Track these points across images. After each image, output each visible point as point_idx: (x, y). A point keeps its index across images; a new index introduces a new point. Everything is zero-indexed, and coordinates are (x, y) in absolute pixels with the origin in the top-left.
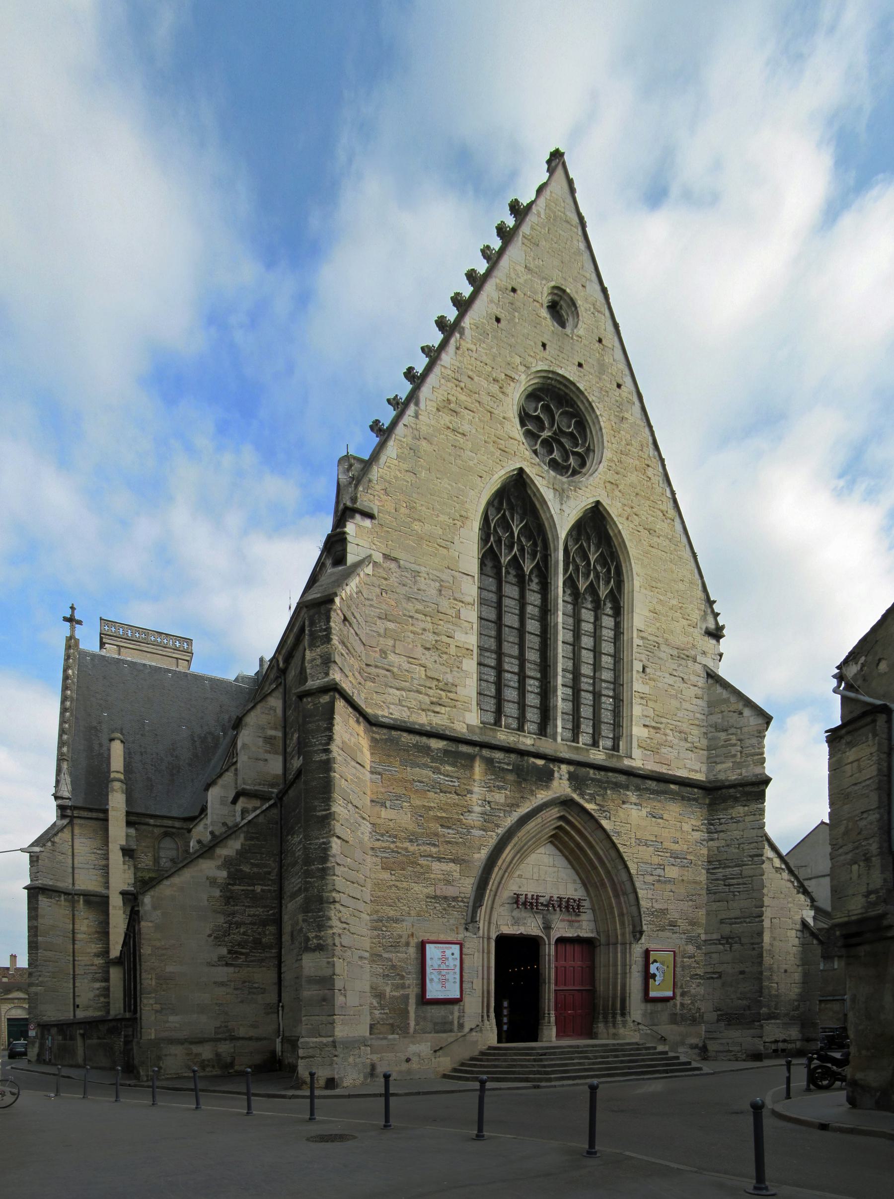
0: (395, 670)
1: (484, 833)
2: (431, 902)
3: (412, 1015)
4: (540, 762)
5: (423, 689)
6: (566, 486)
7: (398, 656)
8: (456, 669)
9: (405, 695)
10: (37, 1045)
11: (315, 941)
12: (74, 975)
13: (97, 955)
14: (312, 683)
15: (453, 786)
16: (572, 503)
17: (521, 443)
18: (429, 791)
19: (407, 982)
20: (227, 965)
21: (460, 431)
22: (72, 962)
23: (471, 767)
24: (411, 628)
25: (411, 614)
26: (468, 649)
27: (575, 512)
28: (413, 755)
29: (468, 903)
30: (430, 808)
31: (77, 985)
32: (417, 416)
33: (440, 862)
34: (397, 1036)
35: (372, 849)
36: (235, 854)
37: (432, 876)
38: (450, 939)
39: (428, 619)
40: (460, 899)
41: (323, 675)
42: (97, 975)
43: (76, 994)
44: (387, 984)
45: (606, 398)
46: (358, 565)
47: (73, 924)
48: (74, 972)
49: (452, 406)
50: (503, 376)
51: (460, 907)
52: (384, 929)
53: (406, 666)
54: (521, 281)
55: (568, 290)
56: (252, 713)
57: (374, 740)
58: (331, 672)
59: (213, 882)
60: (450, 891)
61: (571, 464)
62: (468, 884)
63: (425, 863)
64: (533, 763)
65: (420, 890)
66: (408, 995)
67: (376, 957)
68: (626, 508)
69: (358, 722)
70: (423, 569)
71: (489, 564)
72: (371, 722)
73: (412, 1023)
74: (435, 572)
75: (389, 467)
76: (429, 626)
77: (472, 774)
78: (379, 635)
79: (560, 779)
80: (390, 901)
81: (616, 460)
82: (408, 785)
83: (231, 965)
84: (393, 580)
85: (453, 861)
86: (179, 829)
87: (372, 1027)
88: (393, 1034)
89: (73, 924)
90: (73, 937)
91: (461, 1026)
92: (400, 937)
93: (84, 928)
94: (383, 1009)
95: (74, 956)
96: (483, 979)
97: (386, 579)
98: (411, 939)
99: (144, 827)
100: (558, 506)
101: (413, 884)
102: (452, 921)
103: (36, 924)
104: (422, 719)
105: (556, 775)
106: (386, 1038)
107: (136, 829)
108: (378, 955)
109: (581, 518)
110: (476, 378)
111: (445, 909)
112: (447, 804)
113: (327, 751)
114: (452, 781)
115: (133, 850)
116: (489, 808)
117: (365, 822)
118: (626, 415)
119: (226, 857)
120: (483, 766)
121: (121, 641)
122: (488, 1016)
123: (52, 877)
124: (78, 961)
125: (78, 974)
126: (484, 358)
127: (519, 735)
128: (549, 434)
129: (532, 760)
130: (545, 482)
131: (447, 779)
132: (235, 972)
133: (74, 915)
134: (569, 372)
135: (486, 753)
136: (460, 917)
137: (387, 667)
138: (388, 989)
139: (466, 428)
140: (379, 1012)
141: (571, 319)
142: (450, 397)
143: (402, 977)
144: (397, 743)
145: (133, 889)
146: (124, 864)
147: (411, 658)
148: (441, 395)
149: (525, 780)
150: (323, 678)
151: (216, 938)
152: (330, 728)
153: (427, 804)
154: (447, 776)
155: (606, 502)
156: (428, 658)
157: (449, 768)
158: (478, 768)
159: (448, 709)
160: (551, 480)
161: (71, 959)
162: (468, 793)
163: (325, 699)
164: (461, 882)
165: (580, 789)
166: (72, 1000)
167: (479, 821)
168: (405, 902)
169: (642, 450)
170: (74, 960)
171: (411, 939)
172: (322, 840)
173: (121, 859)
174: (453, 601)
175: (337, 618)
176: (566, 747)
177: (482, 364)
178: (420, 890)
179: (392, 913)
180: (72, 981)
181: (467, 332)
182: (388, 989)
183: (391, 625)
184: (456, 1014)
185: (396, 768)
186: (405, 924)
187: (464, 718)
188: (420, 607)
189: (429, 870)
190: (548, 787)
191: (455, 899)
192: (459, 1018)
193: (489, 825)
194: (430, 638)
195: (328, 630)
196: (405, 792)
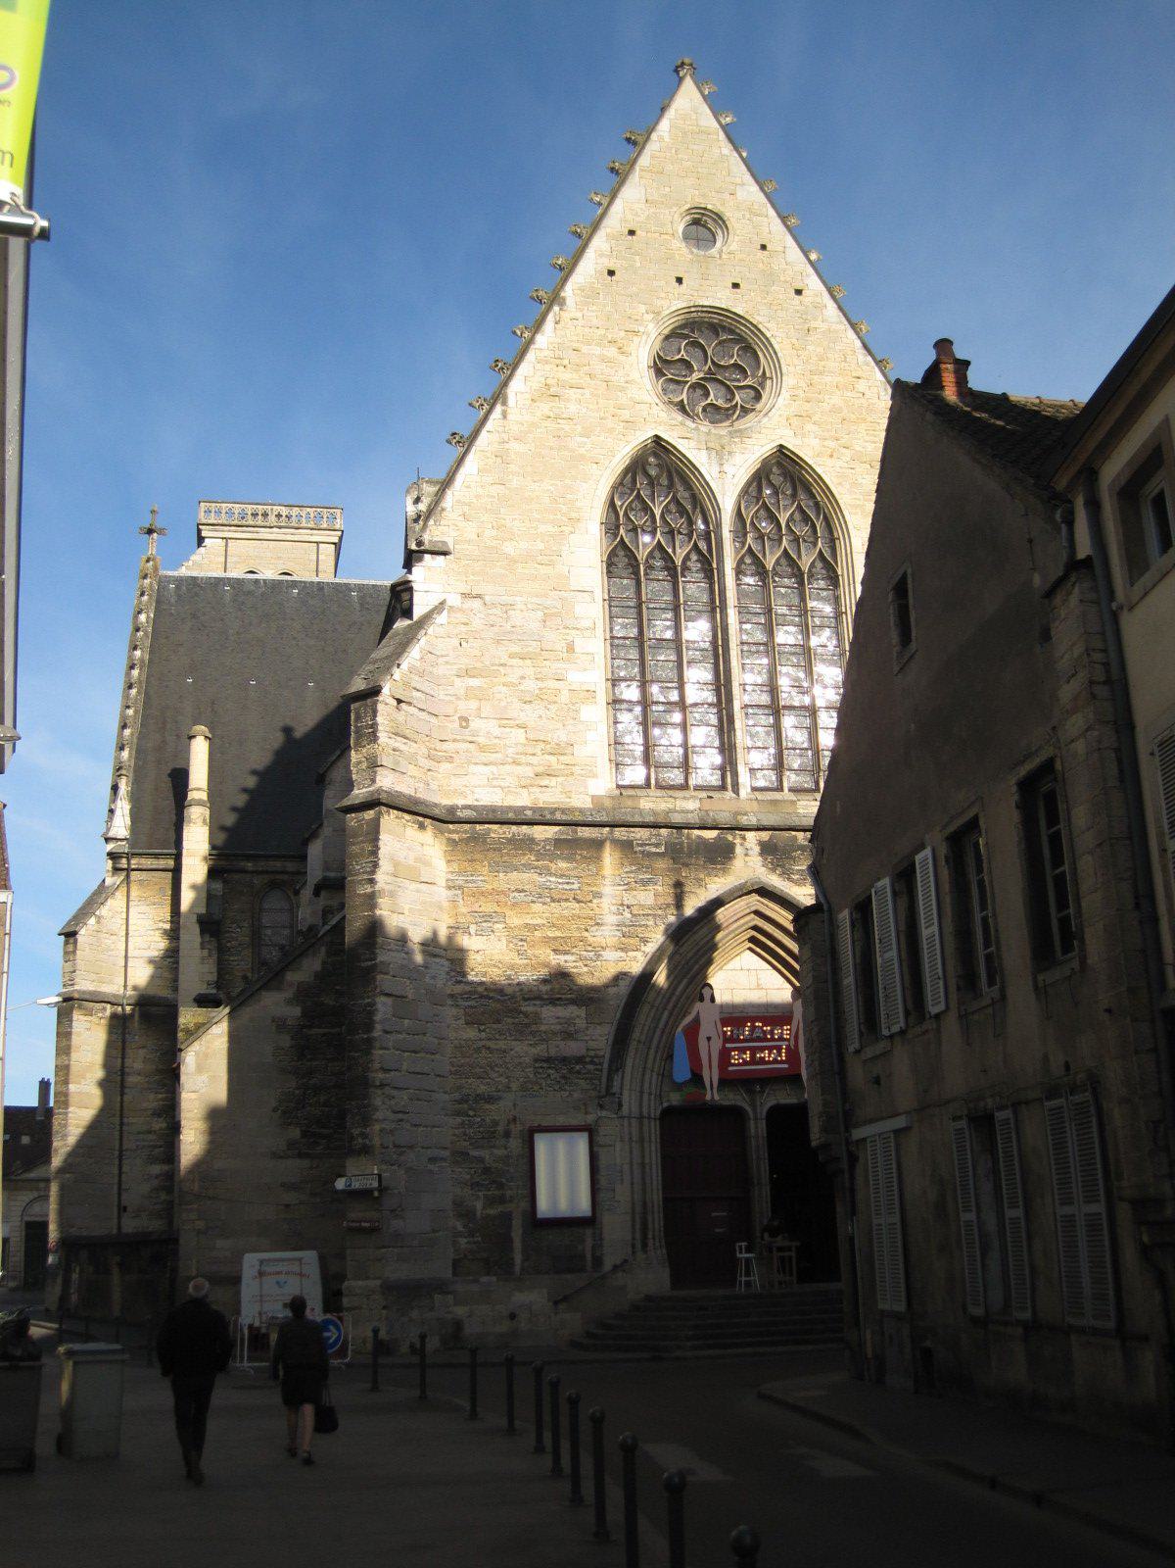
0: (481, 740)
1: (623, 954)
2: (541, 1067)
3: (517, 1244)
4: (710, 835)
5: (523, 759)
6: (725, 441)
7: (486, 721)
8: (571, 722)
9: (495, 772)
10: (59, 1280)
11: (360, 1140)
12: (121, 1151)
13: (157, 1114)
14: (359, 793)
15: (571, 890)
16: (738, 459)
17: (654, 405)
18: (533, 902)
19: (509, 1193)
20: (300, 1156)
21: (564, 416)
22: (118, 1127)
23: (599, 858)
24: (503, 680)
25: (502, 661)
26: (588, 691)
27: (743, 470)
28: (508, 855)
29: (601, 1064)
30: (535, 928)
31: (125, 1169)
32: (504, 415)
33: (555, 1005)
34: (494, 1279)
35: (452, 996)
36: (312, 978)
37: (543, 1028)
38: (574, 1122)
39: (528, 662)
40: (588, 1059)
41: (368, 782)
42: (157, 1150)
43: (123, 1187)
44: (478, 1197)
45: (780, 313)
46: (427, 618)
47: (123, 1058)
48: (121, 1144)
49: (553, 390)
50: (622, 334)
51: (589, 1072)
52: (471, 1113)
53: (497, 731)
54: (642, 218)
55: (709, 207)
56: (339, 764)
57: (452, 842)
58: (378, 778)
59: (280, 1024)
60: (573, 1048)
61: (737, 403)
62: (600, 1036)
63: (530, 1009)
64: (699, 837)
65: (524, 1050)
66: (510, 1213)
67: (461, 1157)
68: (826, 443)
69: (422, 827)
70: (518, 599)
71: (622, 560)
72: (442, 819)
73: (518, 1258)
74: (534, 600)
75: (467, 487)
76: (530, 672)
77: (600, 868)
78: (458, 699)
79: (746, 855)
80: (478, 1070)
81: (805, 385)
82: (502, 898)
83: (307, 1156)
84: (477, 623)
85: (573, 1002)
86: (293, 873)
87: (456, 1264)
88: (488, 1274)
89: (123, 1058)
90: (122, 1081)
91: (598, 1261)
92: (496, 1123)
93: (138, 1065)
94: (473, 1236)
95: (122, 1116)
96: (632, 1184)
97: (466, 624)
98: (512, 1126)
99: (236, 876)
100: (715, 469)
101: (513, 1043)
102: (576, 1095)
103: (66, 1062)
104: (522, 799)
105: (739, 850)
106: (476, 1281)
107: (225, 882)
108: (462, 1153)
109: (759, 469)
110: (585, 349)
111: (564, 1077)
112: (563, 917)
113: (372, 882)
114: (568, 883)
115: (218, 923)
116: (629, 916)
117: (437, 960)
118: (813, 324)
119: (300, 984)
120: (617, 855)
121: (229, 531)
122: (645, 1245)
123: (94, 976)
124: (128, 1124)
125: (127, 1150)
126: (595, 321)
127: (675, 798)
128: (702, 375)
129: (697, 832)
130: (692, 444)
131: (560, 881)
132: (311, 1168)
133: (124, 1042)
134: (720, 297)
135: (620, 833)
136: (588, 1087)
137: (470, 739)
138: (479, 1205)
139: (573, 408)
140: (466, 1240)
141: (719, 232)
142: (549, 381)
143: (501, 1186)
144: (484, 842)
145: (214, 991)
146: (202, 949)
147: (504, 721)
148: (536, 383)
149: (686, 865)
150: (369, 786)
151: (284, 1112)
152: (375, 852)
153: (531, 922)
154: (562, 876)
155: (793, 444)
156: (529, 715)
157: (563, 865)
158: (609, 858)
159: (560, 779)
160: (703, 438)
161: (117, 1121)
162: (594, 897)
163: (370, 814)
164: (588, 1033)
165: (783, 866)
166: (116, 1199)
167: (615, 936)
168: (501, 1070)
169: (845, 361)
170: (122, 1124)
171: (512, 1126)
172: (367, 1001)
173: (198, 939)
174: (564, 631)
175: (387, 708)
176: (755, 803)
177: (591, 330)
178: (524, 1050)
179: (483, 1089)
180: (116, 1162)
181: (569, 302)
182: (479, 1205)
183: (475, 682)
184: (589, 1243)
185: (483, 876)
186: (502, 1103)
187: (586, 787)
188: (516, 649)
189: (537, 1019)
190: (725, 871)
191: (580, 1060)
192: (594, 1248)
193: (632, 941)
194: (530, 685)
195: (374, 726)
196: (498, 909)
